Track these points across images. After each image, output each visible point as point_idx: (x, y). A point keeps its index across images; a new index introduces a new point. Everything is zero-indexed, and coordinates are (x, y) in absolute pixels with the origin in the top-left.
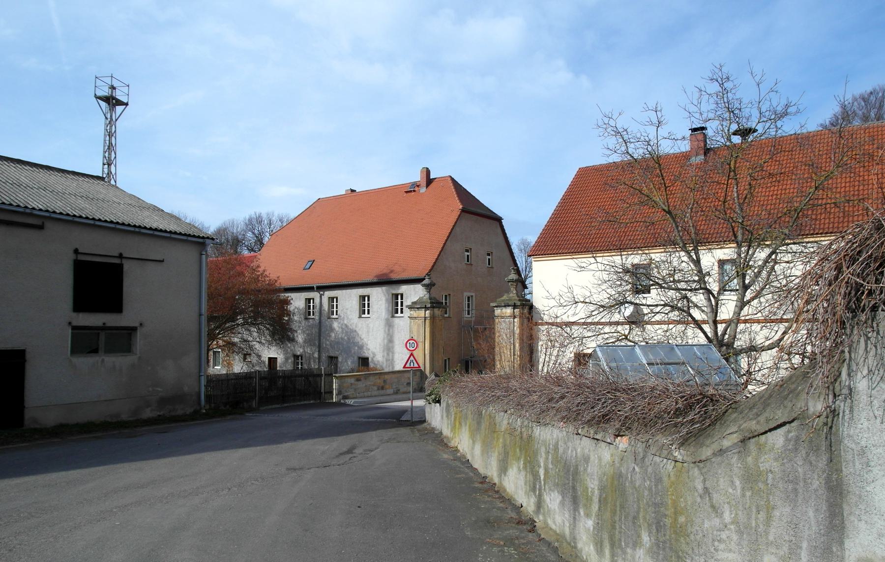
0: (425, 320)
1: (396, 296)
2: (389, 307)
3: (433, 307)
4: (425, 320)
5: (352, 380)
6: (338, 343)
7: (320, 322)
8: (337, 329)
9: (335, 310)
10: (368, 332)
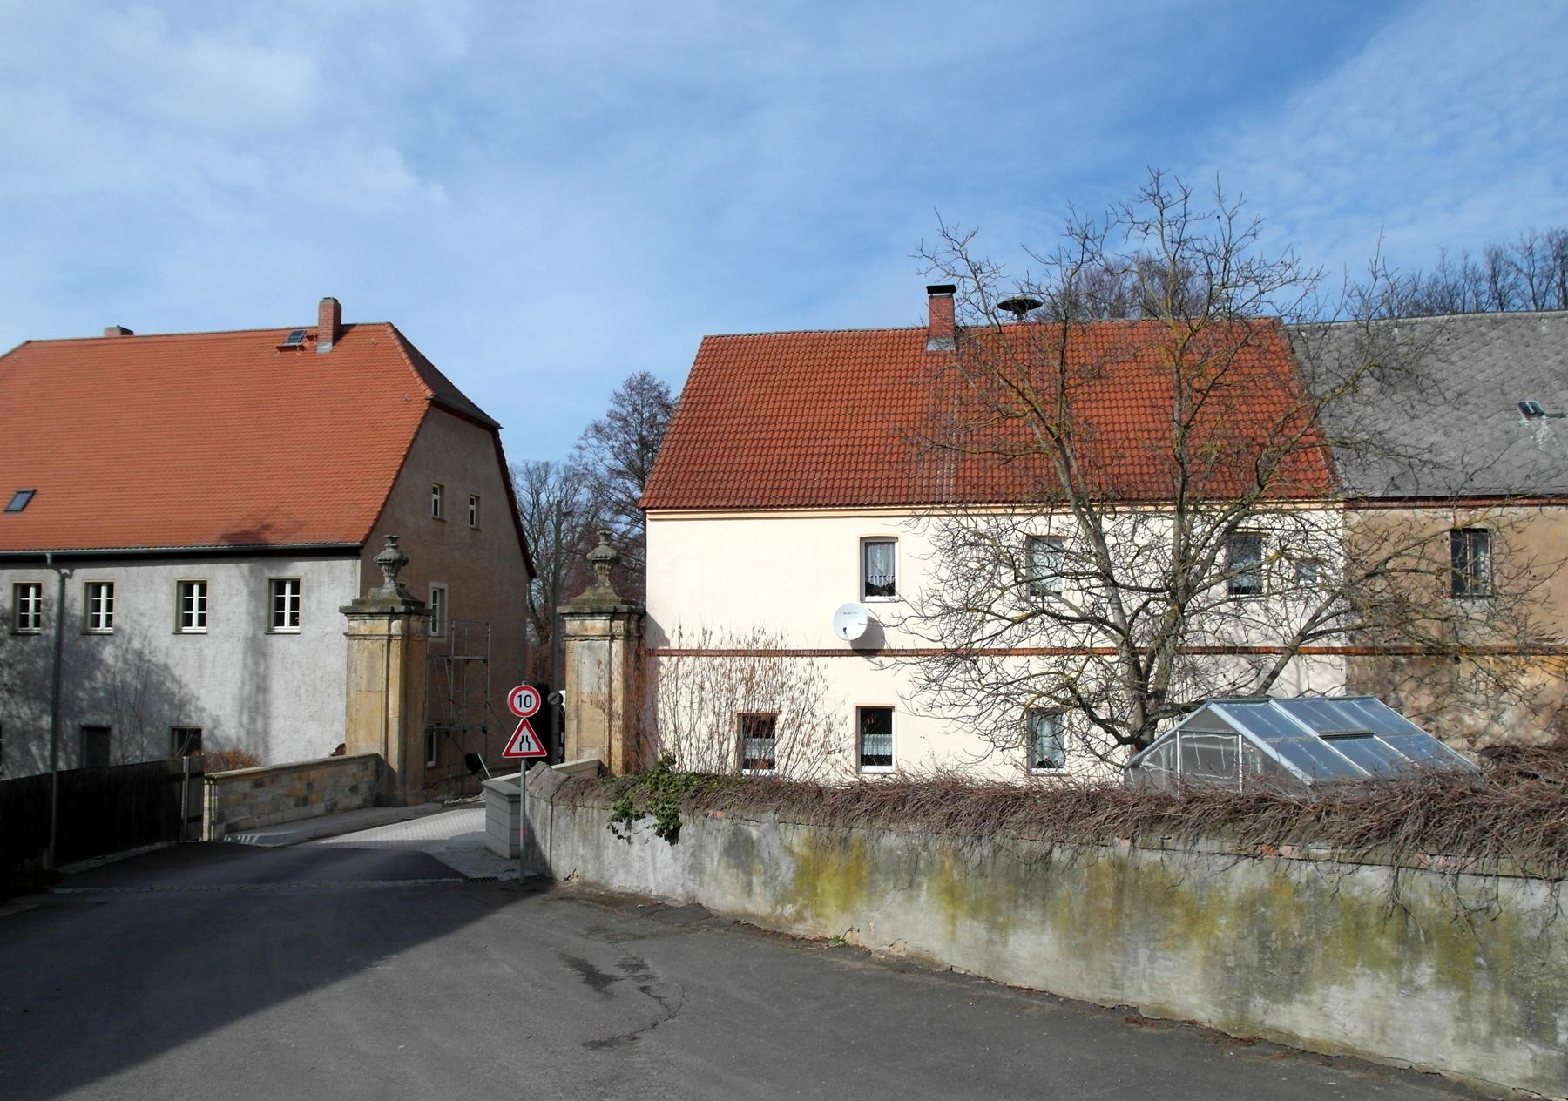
0: (389, 642)
1: (279, 585)
2: (257, 611)
3: (408, 613)
4: (389, 642)
5: (246, 786)
6: (115, 694)
7: (59, 644)
8: (111, 661)
9: (103, 613)
10: (201, 668)
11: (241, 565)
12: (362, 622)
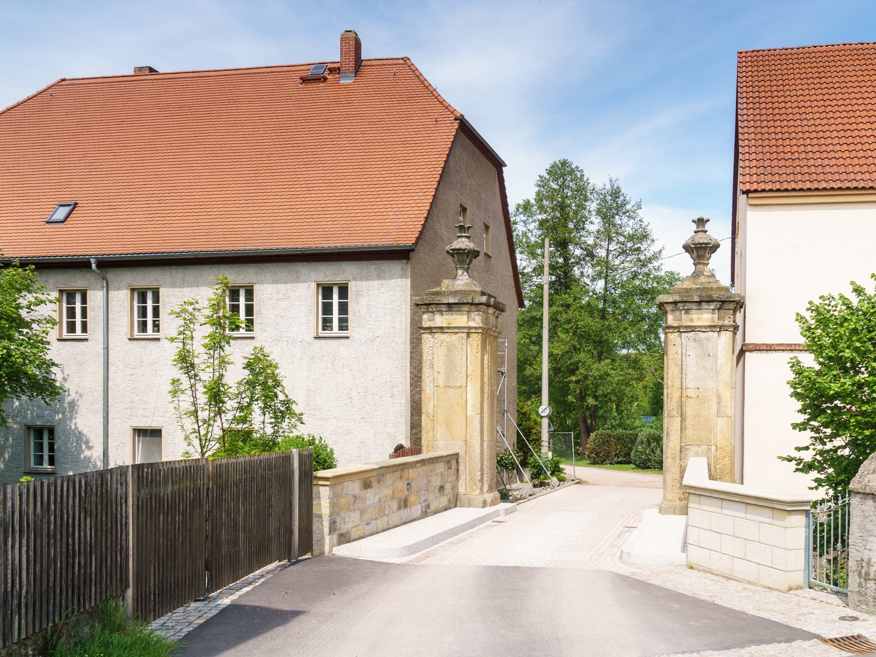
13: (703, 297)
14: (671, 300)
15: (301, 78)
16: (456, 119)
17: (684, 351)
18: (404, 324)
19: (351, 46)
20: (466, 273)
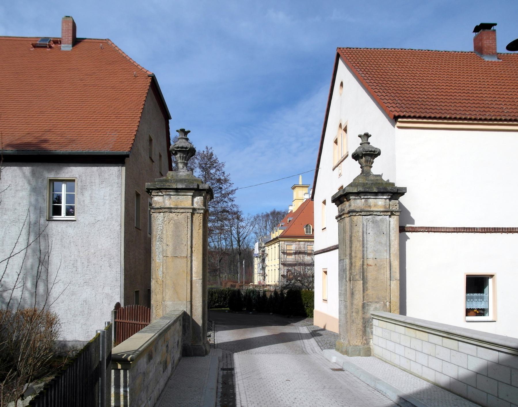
0: (193, 214)
4: (193, 214)
11: (24, 168)
12: (167, 198)
13: (380, 189)
14: (355, 191)
15: (32, 44)
16: (149, 76)
17: (365, 230)
18: (119, 211)
19: (69, 26)
20: (185, 168)
